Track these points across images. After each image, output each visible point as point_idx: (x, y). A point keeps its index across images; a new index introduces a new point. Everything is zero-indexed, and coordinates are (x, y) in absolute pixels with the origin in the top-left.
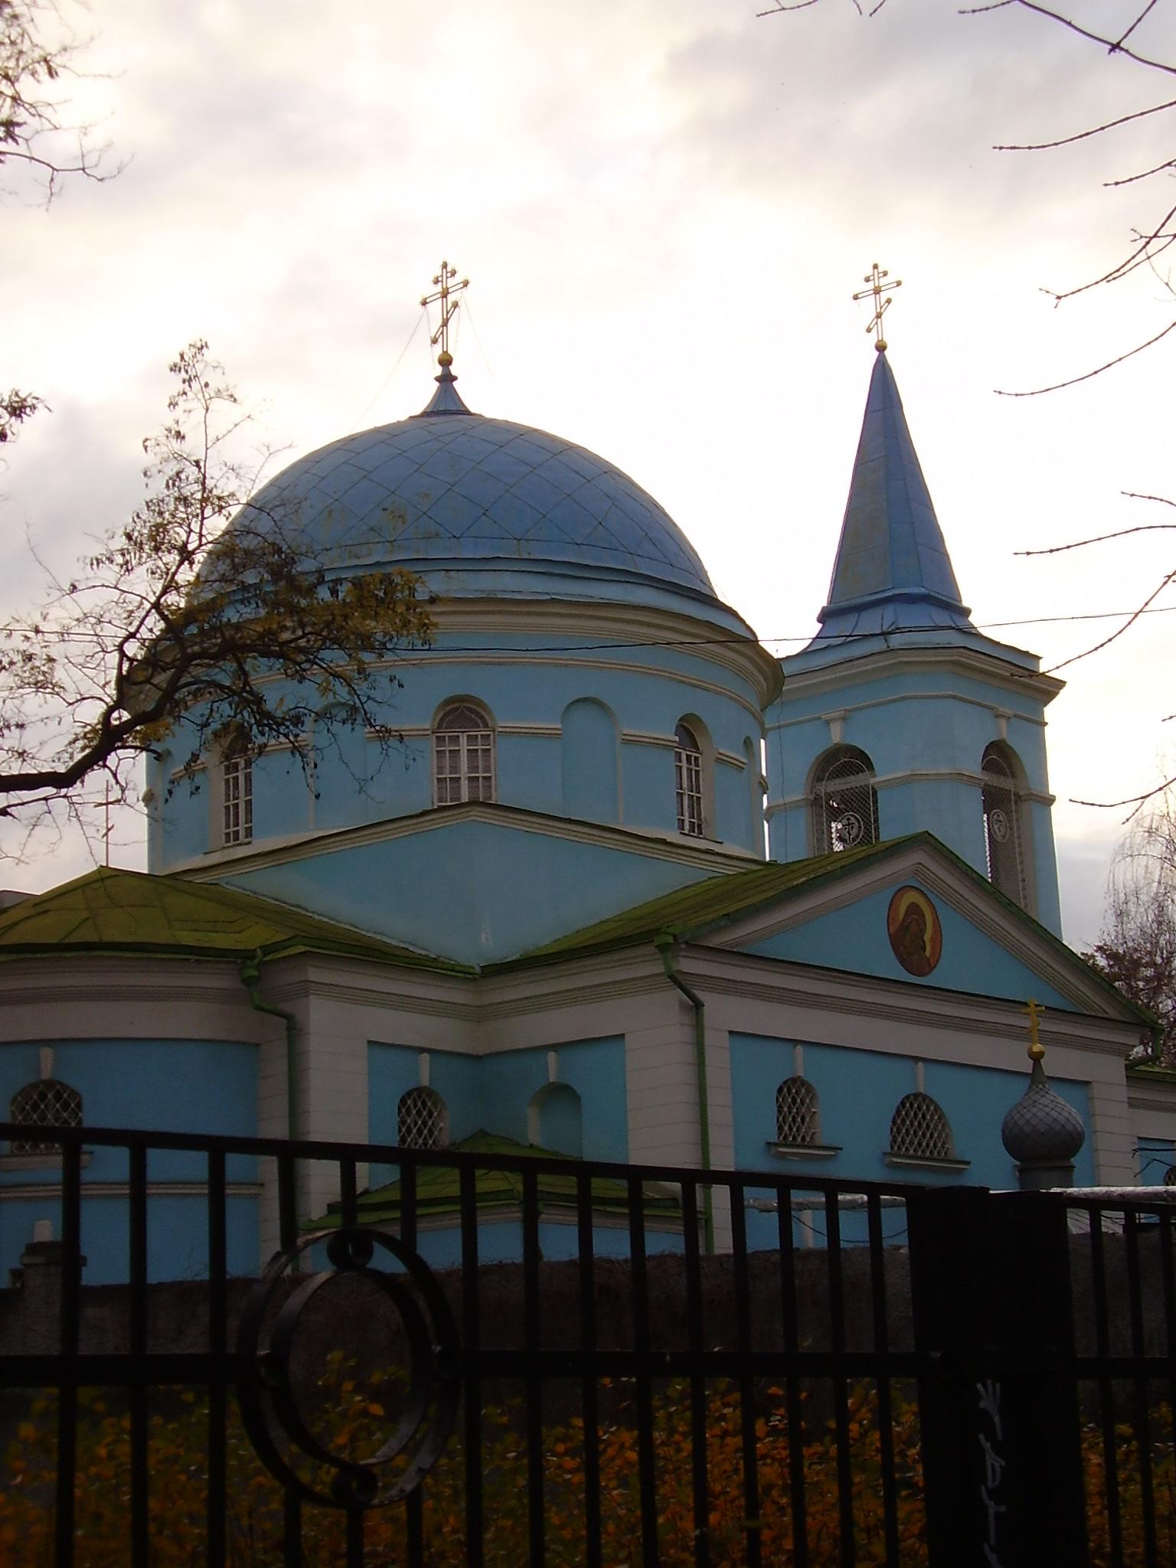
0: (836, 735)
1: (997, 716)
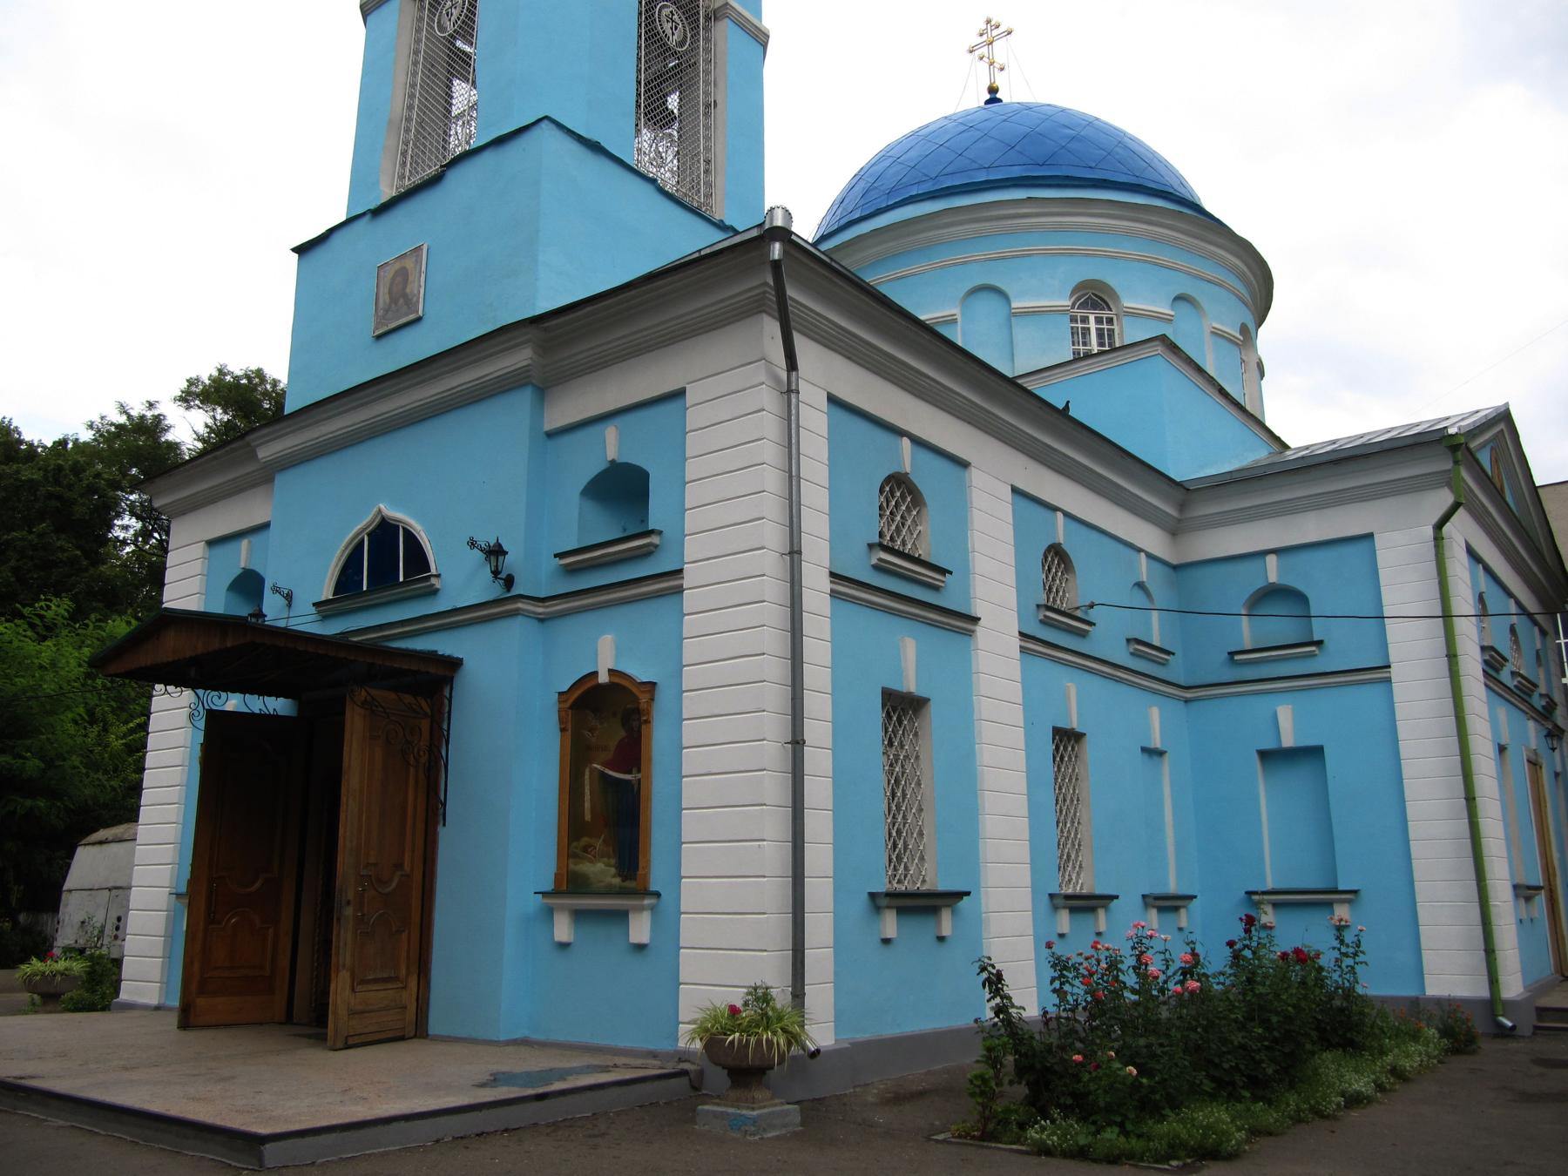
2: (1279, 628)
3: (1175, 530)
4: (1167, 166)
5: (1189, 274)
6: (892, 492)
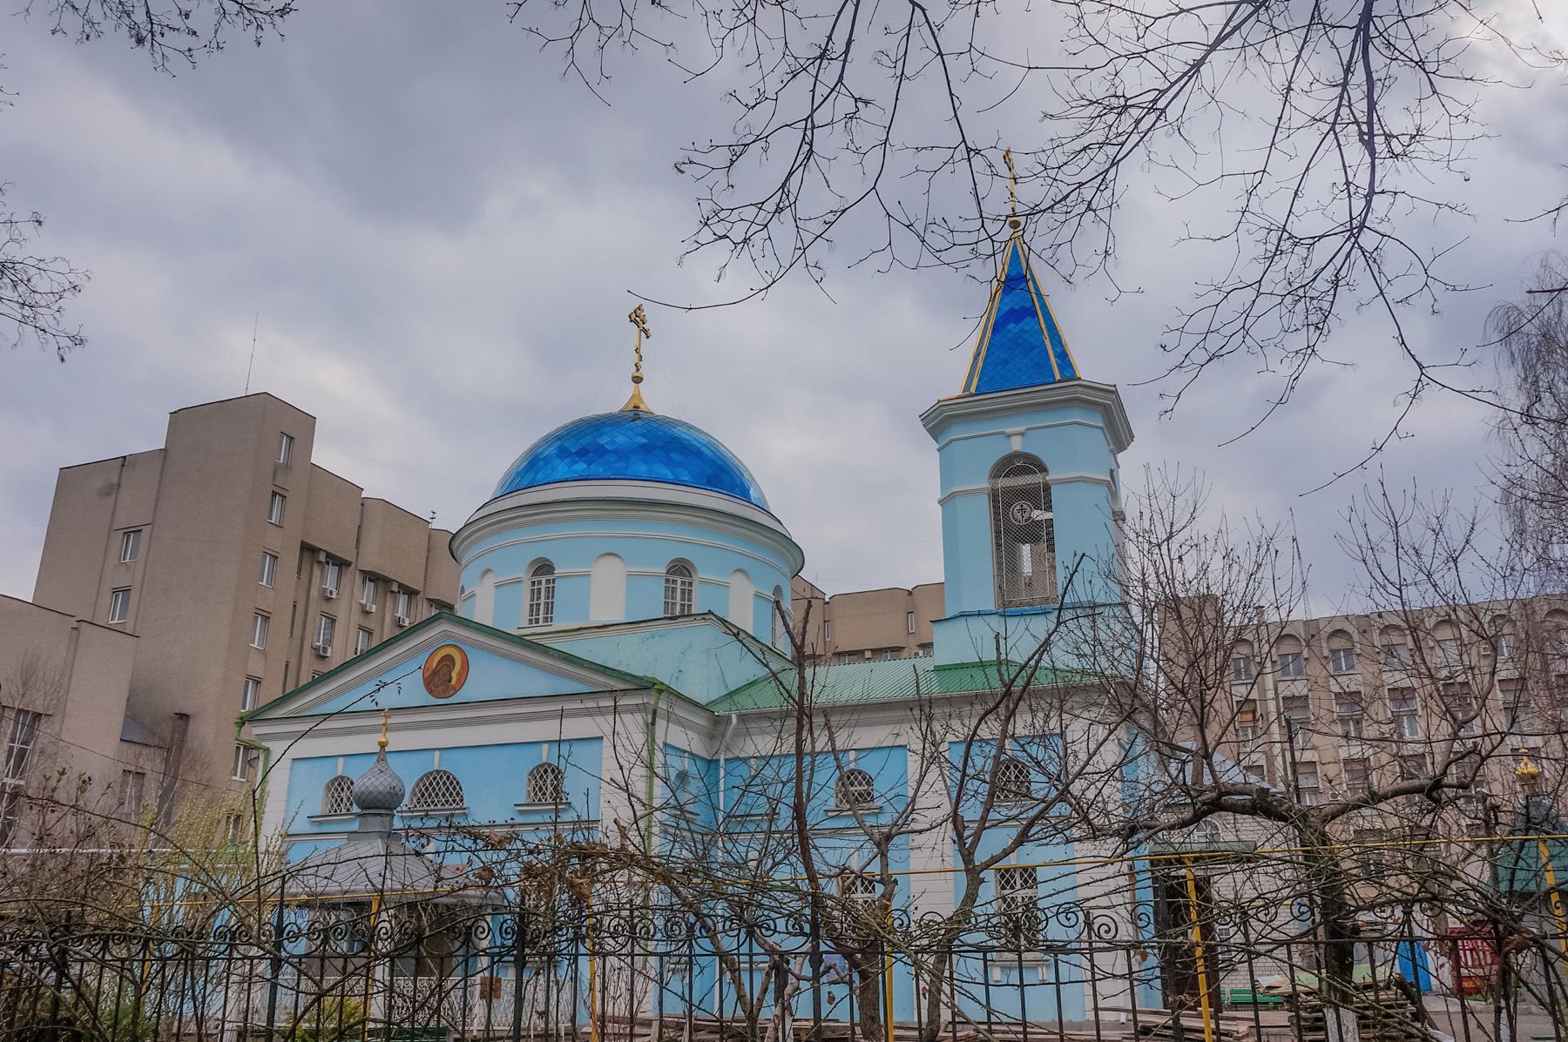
0: (1017, 445)
1: (1009, 436)
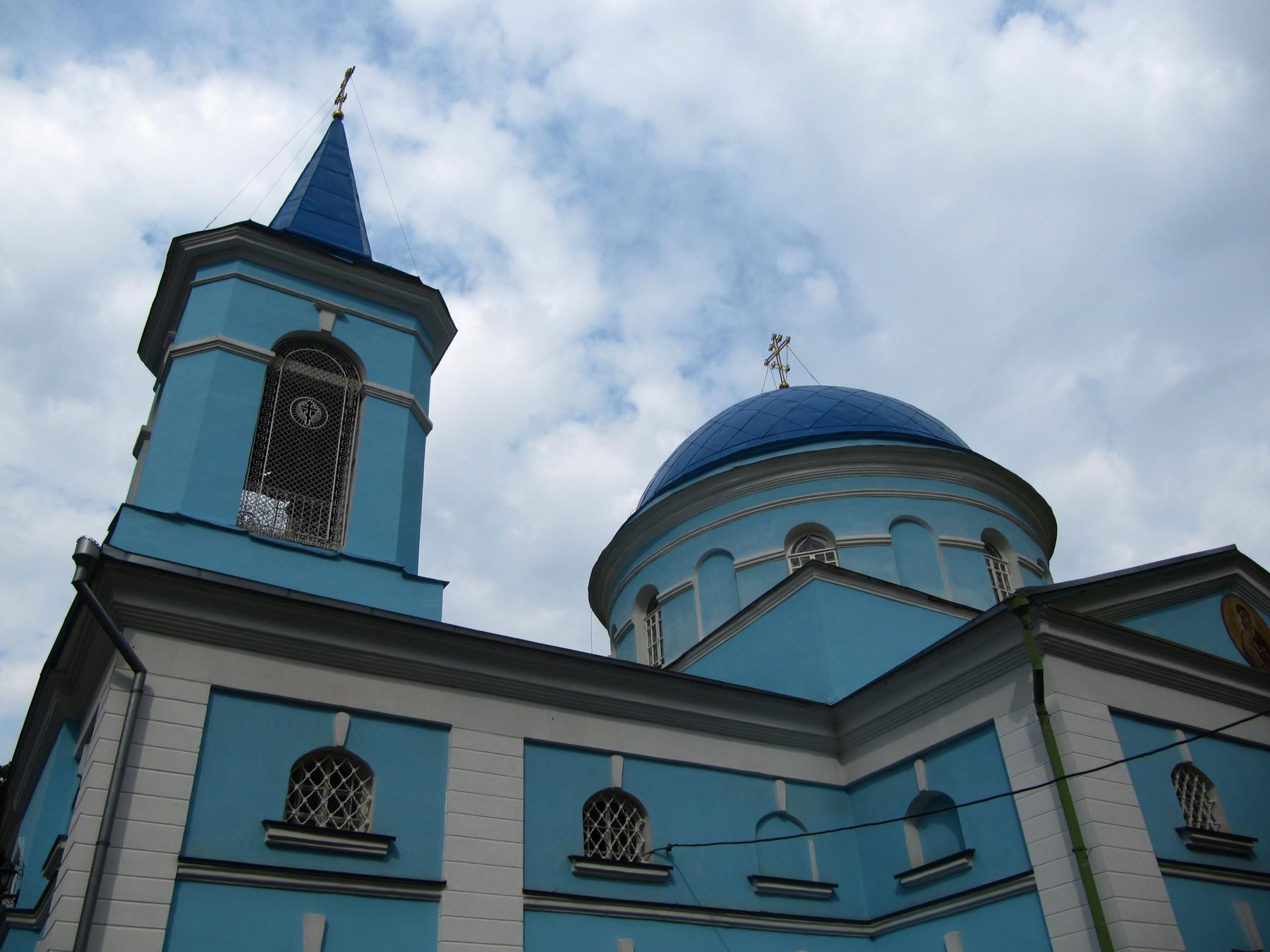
0: (326, 322)
2: (940, 839)
3: (840, 751)
4: (884, 402)
5: (903, 496)
6: (1182, 778)
